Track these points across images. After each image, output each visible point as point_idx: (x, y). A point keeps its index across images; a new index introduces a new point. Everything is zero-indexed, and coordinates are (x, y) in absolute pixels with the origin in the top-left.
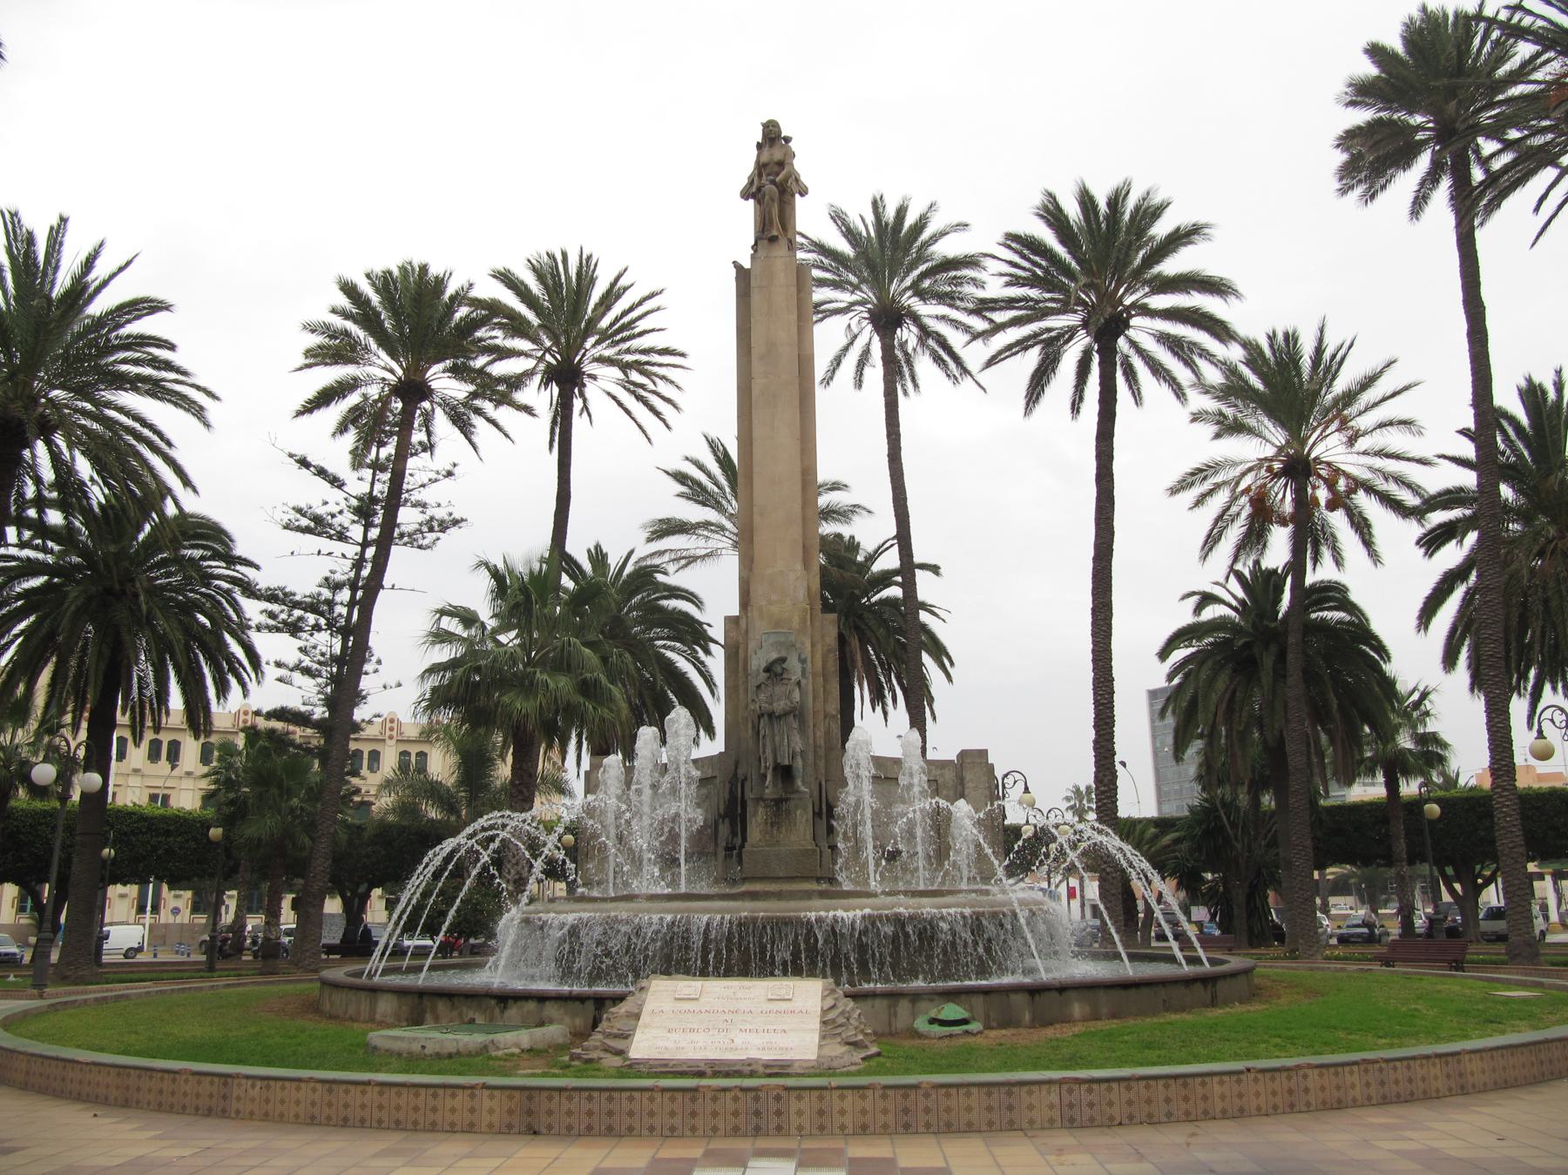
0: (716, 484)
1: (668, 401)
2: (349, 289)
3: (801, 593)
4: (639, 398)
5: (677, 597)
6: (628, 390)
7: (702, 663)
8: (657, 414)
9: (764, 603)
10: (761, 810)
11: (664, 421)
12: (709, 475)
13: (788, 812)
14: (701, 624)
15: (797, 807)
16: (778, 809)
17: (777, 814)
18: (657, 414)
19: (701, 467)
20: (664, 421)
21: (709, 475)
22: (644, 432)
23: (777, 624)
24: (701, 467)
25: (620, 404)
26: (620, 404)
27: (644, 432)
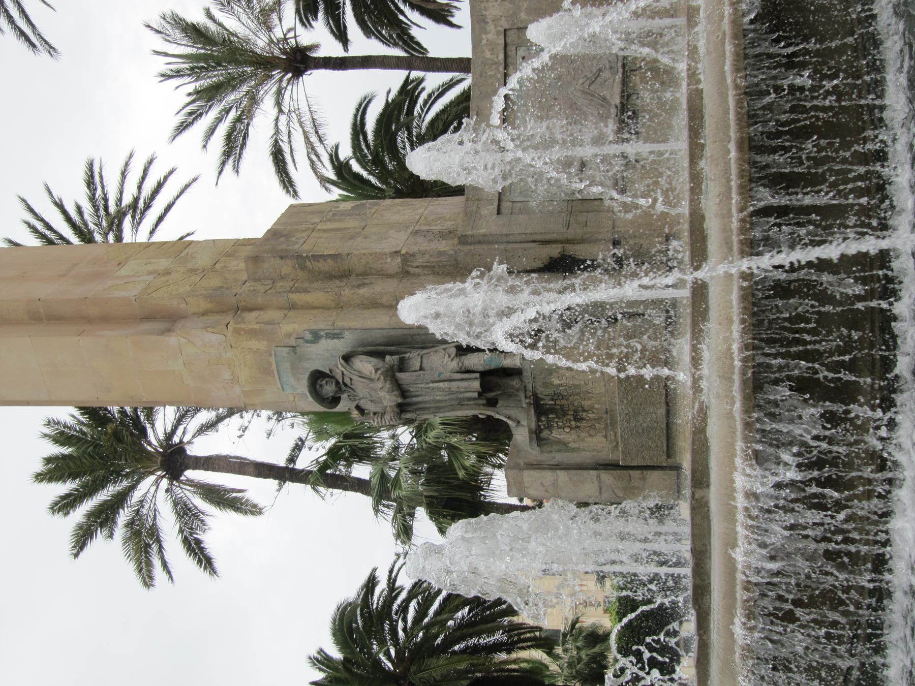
0: (227, 111)
1: (145, 172)
2: (83, 537)
3: (214, 338)
4: (148, 206)
5: (363, 124)
6: (141, 219)
7: (430, 96)
8: (160, 185)
9: (237, 390)
10: (556, 434)
11: (166, 178)
12: (219, 120)
13: (556, 396)
14: (387, 105)
15: (547, 385)
16: (552, 410)
17: (561, 412)
18: (160, 185)
19: (212, 131)
20: (166, 178)
21: (219, 120)
22: (187, 186)
23: (266, 371)
24: (212, 131)
25: (161, 219)
26: (161, 219)
27: (187, 186)
